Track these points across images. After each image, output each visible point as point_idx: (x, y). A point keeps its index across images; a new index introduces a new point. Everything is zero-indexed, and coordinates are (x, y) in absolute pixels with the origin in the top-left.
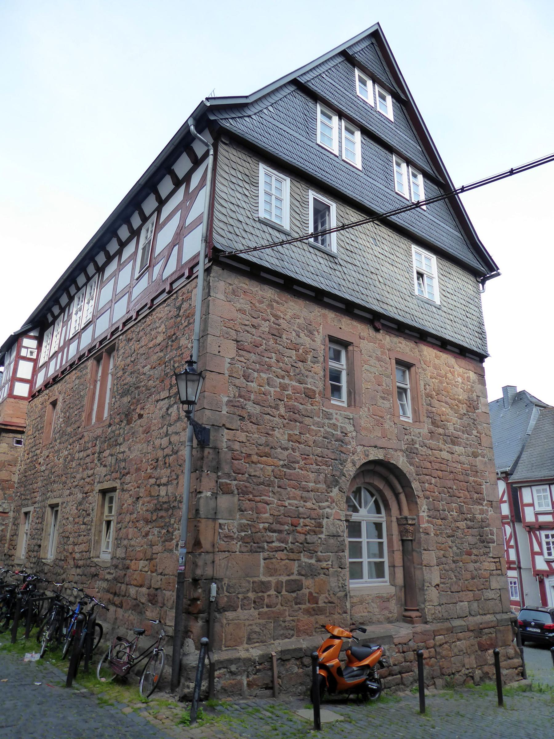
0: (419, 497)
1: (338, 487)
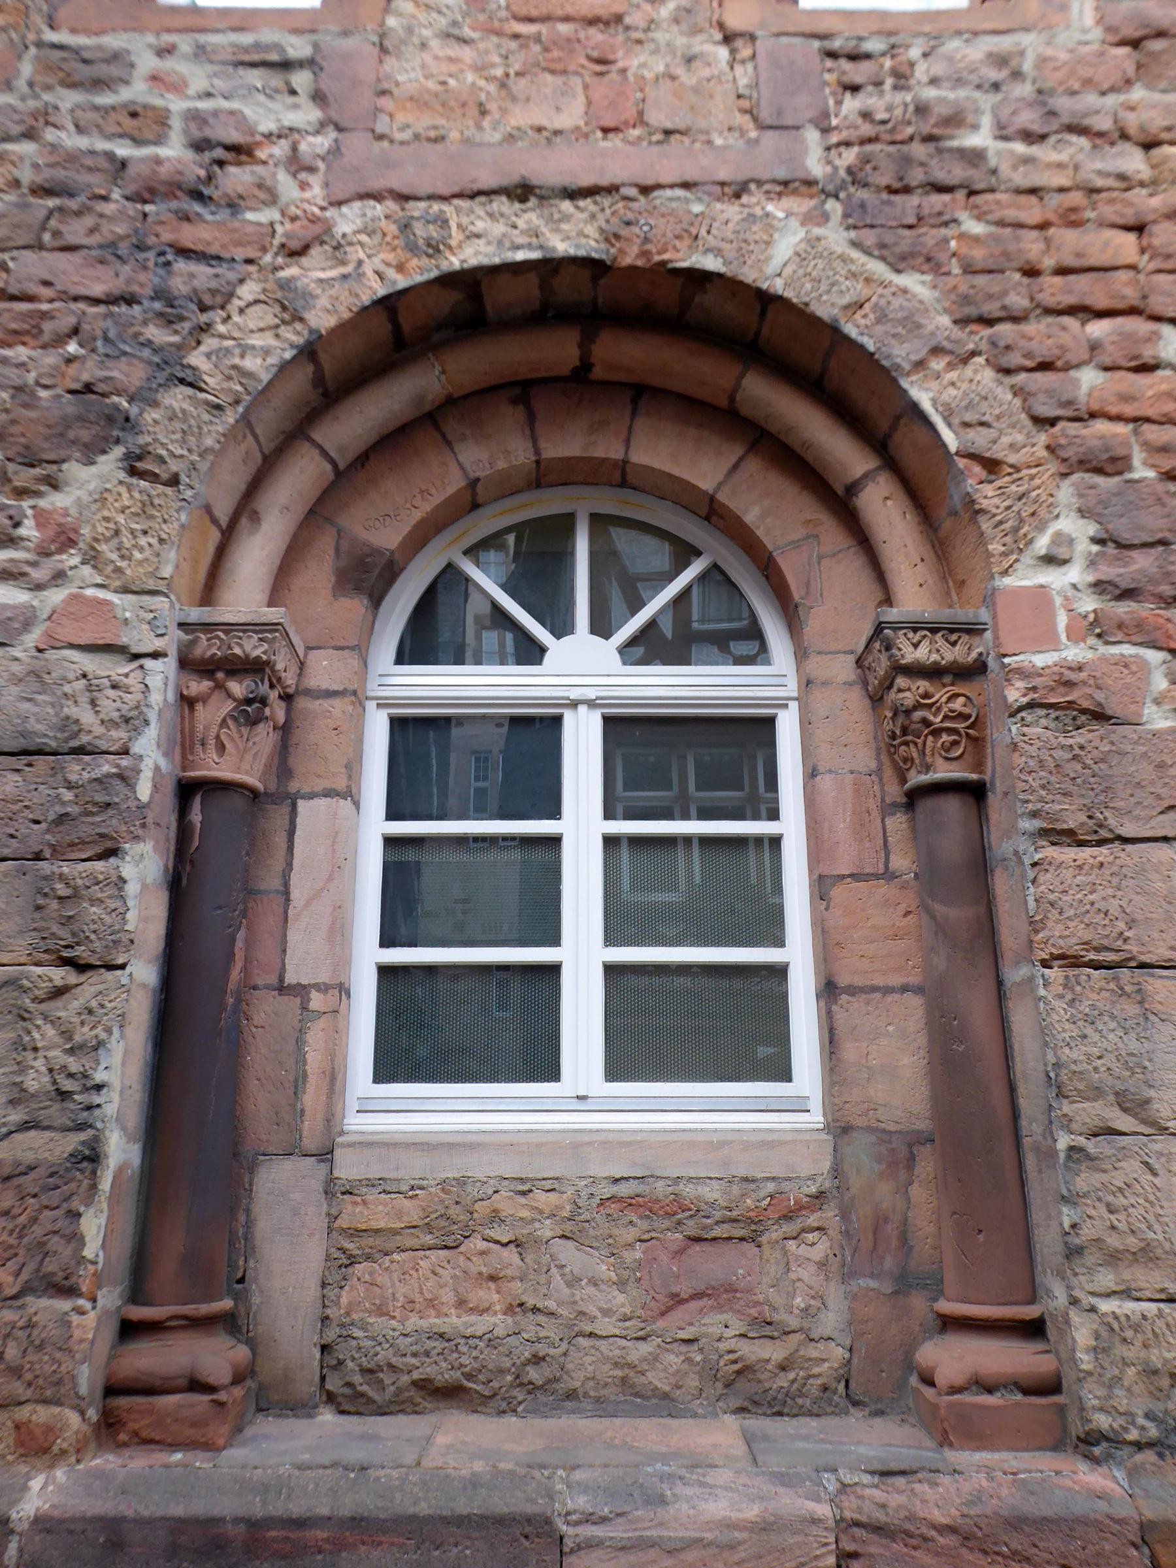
0: (992, 466)
1: (118, 451)
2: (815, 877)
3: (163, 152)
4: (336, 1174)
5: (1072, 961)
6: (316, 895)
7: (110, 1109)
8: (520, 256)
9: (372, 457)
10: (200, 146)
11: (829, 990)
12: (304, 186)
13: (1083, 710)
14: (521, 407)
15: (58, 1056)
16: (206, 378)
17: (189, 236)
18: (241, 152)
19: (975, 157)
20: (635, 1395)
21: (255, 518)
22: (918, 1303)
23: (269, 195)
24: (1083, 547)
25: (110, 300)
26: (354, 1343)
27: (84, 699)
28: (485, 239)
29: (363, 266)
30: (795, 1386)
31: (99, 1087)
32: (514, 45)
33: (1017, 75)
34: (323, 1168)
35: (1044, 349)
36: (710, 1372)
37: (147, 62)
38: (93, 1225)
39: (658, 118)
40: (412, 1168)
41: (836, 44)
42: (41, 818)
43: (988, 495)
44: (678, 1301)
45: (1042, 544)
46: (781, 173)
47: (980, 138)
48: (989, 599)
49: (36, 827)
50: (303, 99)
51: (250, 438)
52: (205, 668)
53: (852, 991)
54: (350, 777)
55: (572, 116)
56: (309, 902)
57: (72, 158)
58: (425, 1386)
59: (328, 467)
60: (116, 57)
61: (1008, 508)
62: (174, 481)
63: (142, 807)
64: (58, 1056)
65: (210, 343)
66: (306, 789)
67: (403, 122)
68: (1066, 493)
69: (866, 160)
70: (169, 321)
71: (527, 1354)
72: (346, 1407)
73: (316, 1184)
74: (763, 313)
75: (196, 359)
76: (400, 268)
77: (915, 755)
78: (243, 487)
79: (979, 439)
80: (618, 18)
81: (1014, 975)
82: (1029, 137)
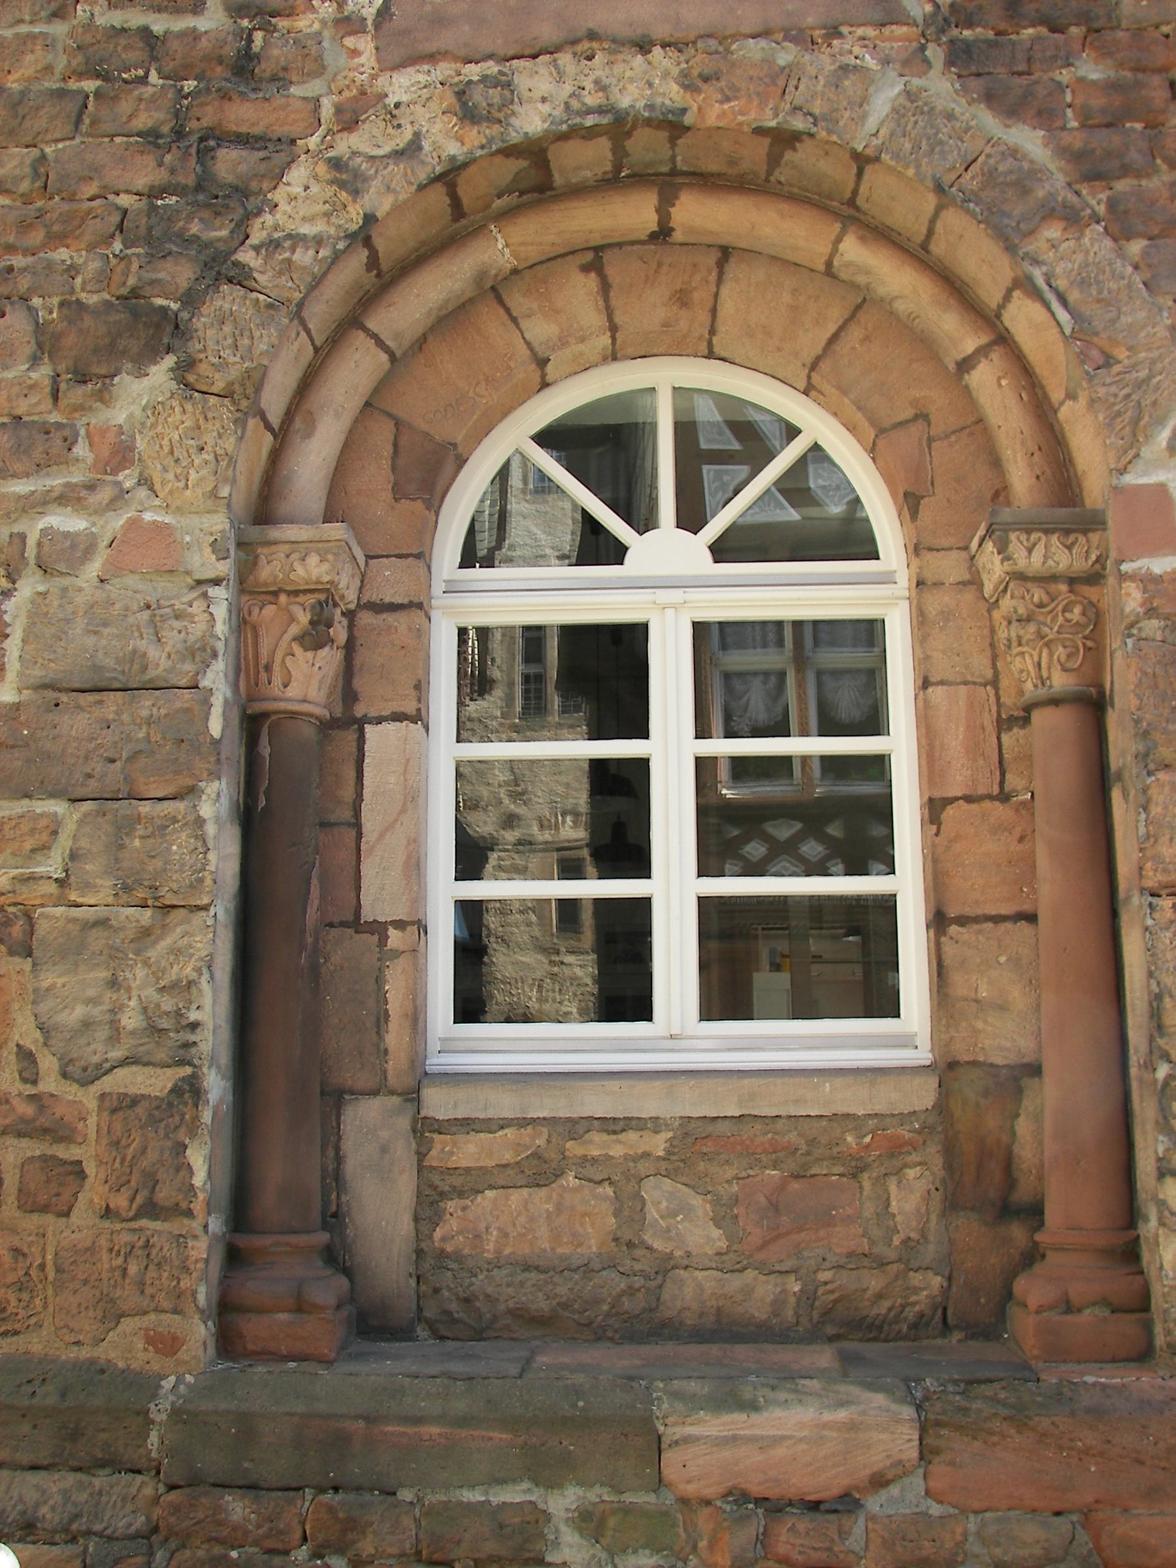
1: (170, 360)
2: (926, 799)
3: (202, 24)
4: (423, 1113)
6: (391, 827)
7: (206, 1047)
9: (430, 338)
11: (939, 921)
14: (593, 275)
16: (255, 275)
26: (449, 1274)
27: (148, 631)
30: (892, 1314)
31: (194, 1026)
34: (410, 1108)
38: (198, 1159)
40: (648, 1103)
42: (117, 756)
49: (112, 766)
51: (303, 334)
53: (962, 921)
54: (419, 700)
56: (382, 835)
59: (384, 357)
61: (1128, 396)
63: (216, 743)
66: (373, 713)
71: (622, 1285)
72: (445, 1333)
73: (404, 1123)
74: (860, 174)
75: (246, 256)
77: (1031, 668)
78: (294, 385)
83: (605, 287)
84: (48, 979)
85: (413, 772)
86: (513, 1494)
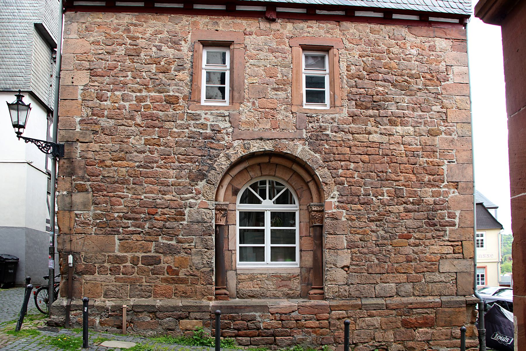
0: (326, 184)
1: (205, 180)
5: (330, 249)
8: (261, 150)
10: (212, 130)
12: (229, 137)
13: (334, 218)
15: (207, 260)
17: (212, 146)
18: (219, 131)
19: (327, 135)
20: (275, 297)
21: (222, 186)
22: (309, 287)
23: (224, 139)
24: (337, 196)
25: (202, 156)
28: (256, 147)
29: (238, 151)
32: (259, 113)
33: (335, 121)
35: (335, 166)
36: (284, 294)
37: (204, 116)
39: (281, 127)
40: (247, 272)
41: (308, 115)
43: (325, 188)
44: (280, 287)
45: (332, 195)
46: (299, 137)
47: (328, 132)
48: (325, 202)
50: (227, 122)
52: (218, 210)
53: (304, 251)
55: (268, 126)
57: (194, 132)
58: (249, 296)
60: (199, 115)
62: (214, 185)
64: (207, 260)
65: (216, 163)
67: (243, 127)
68: (335, 188)
69: (312, 135)
70: (210, 159)
76: (244, 152)
79: (325, 180)
80: (276, 109)
81: (324, 250)
82: (336, 132)
83: (261, 168)
84: (193, 257)
85: (235, 231)
86: (252, 313)
